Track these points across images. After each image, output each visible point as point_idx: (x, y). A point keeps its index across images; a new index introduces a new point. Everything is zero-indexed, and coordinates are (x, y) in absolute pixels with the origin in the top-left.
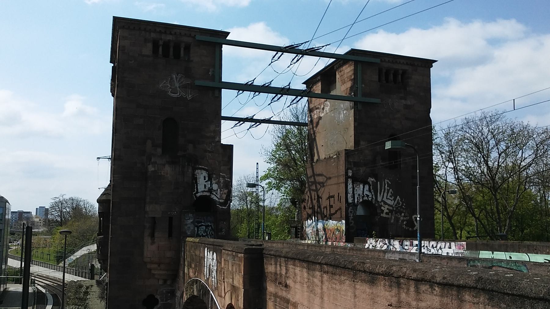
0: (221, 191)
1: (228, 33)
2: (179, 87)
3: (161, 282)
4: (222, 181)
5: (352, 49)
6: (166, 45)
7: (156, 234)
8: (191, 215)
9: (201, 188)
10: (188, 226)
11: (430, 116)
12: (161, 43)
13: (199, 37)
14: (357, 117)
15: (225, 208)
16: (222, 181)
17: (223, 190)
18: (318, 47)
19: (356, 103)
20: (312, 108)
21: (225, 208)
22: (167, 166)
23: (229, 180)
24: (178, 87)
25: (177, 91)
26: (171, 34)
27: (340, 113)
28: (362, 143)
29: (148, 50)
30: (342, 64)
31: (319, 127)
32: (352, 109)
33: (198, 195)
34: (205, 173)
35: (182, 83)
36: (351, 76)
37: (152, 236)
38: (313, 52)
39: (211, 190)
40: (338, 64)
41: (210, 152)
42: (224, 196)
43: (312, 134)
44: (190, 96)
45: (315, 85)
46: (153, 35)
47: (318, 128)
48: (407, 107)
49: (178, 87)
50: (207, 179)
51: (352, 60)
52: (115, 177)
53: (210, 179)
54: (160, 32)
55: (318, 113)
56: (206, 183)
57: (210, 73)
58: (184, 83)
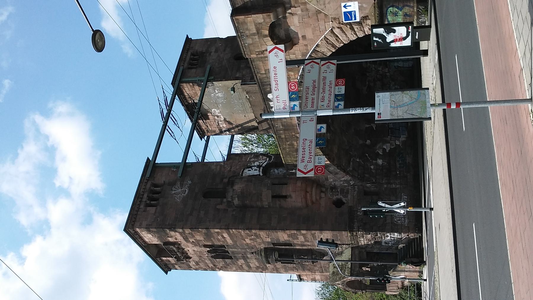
0: (260, 160)
1: (148, 159)
2: (181, 189)
3: (323, 195)
4: (253, 159)
5: (171, 84)
6: (151, 199)
7: (284, 194)
8: (272, 170)
9: (256, 173)
10: (279, 172)
11: (225, 38)
12: (148, 202)
13: (148, 175)
14: (219, 79)
15: (273, 157)
16: (253, 159)
17: (260, 159)
18: (196, 159)
19: (208, 80)
20: (219, 130)
21: (273, 157)
22: (234, 188)
23: (253, 155)
24: (181, 190)
25: (184, 190)
26: (143, 195)
27: (218, 97)
28: (237, 76)
29: (152, 210)
30: (183, 96)
31: (232, 121)
32: (213, 83)
33: (261, 174)
34: (246, 171)
35: (178, 187)
36: (190, 86)
37: (285, 197)
38: (170, 107)
39: (259, 167)
40: (183, 100)
41: (231, 168)
42: (264, 157)
43: (238, 129)
44: (189, 182)
45: (201, 127)
46: (142, 206)
47: (233, 122)
48: (216, 51)
49: (181, 190)
50: (250, 169)
51: (179, 84)
52: (241, 228)
53: (251, 167)
54: (141, 202)
55: (221, 123)
56: (253, 170)
57: (175, 170)
58: (179, 186)
